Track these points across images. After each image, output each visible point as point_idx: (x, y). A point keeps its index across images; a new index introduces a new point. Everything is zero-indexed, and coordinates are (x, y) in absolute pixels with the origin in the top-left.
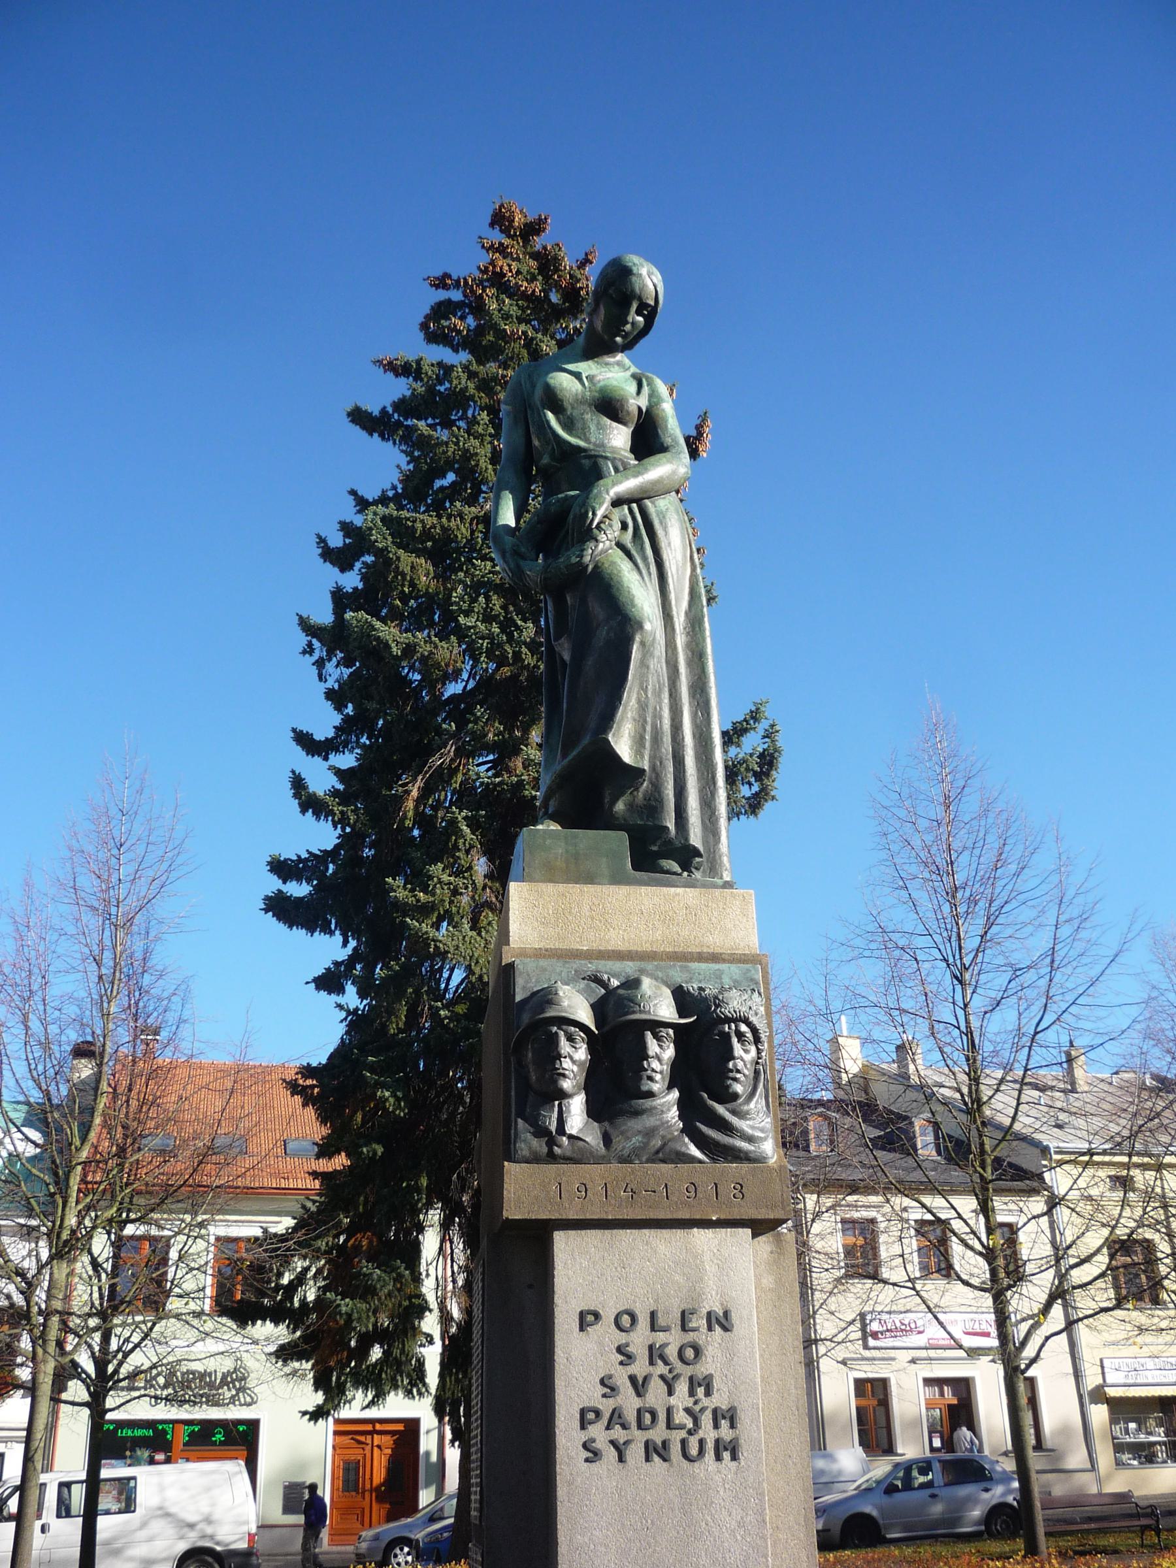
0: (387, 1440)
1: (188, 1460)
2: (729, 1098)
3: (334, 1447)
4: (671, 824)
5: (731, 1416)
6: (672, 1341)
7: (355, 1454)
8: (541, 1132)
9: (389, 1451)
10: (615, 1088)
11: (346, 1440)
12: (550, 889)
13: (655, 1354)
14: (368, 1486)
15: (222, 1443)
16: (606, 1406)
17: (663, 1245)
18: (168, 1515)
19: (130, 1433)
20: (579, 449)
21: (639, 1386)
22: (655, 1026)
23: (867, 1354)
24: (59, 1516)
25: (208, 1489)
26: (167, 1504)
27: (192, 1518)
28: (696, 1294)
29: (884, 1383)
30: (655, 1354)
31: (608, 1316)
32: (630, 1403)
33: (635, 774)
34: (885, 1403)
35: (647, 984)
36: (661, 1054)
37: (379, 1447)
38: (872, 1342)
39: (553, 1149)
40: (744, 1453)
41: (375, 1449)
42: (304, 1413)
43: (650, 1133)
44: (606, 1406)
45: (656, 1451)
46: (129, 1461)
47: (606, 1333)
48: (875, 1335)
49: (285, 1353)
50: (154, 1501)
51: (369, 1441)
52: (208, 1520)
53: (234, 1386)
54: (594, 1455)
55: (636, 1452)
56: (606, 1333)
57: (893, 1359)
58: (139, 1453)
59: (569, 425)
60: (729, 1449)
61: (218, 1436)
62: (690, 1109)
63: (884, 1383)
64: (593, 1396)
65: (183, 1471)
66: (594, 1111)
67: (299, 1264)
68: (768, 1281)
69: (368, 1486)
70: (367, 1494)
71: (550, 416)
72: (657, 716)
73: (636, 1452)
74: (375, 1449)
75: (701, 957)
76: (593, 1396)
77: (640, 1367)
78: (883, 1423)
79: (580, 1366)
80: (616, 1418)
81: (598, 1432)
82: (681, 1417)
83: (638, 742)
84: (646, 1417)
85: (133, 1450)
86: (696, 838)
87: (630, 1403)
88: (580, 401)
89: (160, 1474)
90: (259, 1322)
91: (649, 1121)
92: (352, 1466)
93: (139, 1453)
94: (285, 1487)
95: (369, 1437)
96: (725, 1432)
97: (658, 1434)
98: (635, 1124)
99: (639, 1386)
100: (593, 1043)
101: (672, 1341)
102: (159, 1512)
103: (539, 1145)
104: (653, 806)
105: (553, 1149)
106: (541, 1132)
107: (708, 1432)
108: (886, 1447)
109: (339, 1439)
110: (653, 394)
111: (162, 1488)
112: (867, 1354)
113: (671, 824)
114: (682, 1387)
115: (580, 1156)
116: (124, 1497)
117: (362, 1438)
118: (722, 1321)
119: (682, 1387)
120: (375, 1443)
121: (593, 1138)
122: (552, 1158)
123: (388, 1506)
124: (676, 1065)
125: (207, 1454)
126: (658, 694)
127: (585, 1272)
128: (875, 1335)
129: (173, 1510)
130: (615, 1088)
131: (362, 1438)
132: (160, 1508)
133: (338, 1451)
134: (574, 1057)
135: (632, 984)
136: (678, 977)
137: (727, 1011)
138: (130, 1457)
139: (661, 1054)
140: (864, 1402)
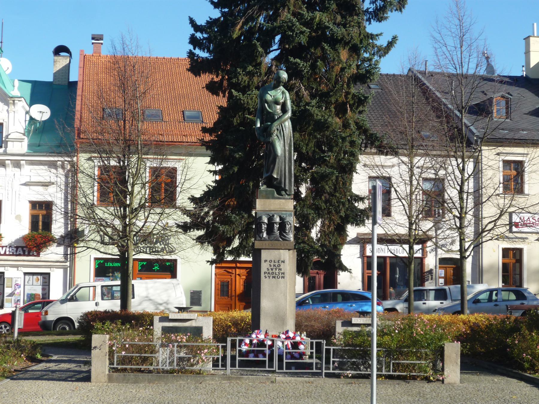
0: (244, 272)
1: (141, 279)
2: (286, 233)
3: (215, 274)
4: (283, 186)
5: (284, 273)
6: (277, 264)
7: (227, 278)
8: (260, 237)
9: (244, 277)
10: (270, 230)
11: (222, 271)
12: (262, 200)
13: (274, 266)
14: (233, 294)
15: (158, 271)
16: (268, 272)
17: (276, 252)
18: (150, 300)
19: (111, 265)
20: (271, 112)
21: (272, 269)
22: (276, 223)
23: (511, 235)
24: (102, 299)
25: (166, 290)
26: (149, 295)
27: (161, 302)
28: (280, 258)
29: (520, 251)
30: (274, 266)
31: (268, 261)
32: (271, 271)
33: (277, 179)
34: (520, 261)
35: (275, 216)
36: (276, 226)
37: (239, 275)
38: (514, 229)
39: (261, 239)
40: (285, 278)
41: (237, 276)
42: (208, 262)
43: (275, 237)
44: (268, 272)
45: (274, 277)
46: (111, 278)
47: (268, 263)
48: (517, 225)
49: (200, 240)
50: (144, 294)
51: (234, 272)
52: (167, 303)
53: (163, 243)
54: (266, 277)
55: (271, 277)
56: (268, 263)
57: (527, 238)
58: (116, 274)
59: (269, 107)
60: (283, 277)
61: (156, 267)
62: (281, 234)
63: (520, 251)
64: (266, 270)
65: (156, 282)
66: (267, 234)
67: (206, 209)
68: (291, 256)
69: (233, 294)
70: (233, 298)
71: (266, 105)
72: (281, 167)
73: (271, 277)
74: (237, 276)
75: (284, 211)
76: (266, 270)
77: (272, 267)
78: (518, 272)
79: (264, 267)
80: (269, 273)
81: (266, 275)
82: (277, 273)
83: (277, 174)
84: (273, 273)
85: (113, 273)
86: (287, 188)
87: (271, 271)
88: (271, 102)
89: (146, 283)
90: (192, 230)
91: (274, 236)
92: (225, 284)
93: (116, 274)
94: (191, 293)
95: (234, 270)
96: (283, 275)
97: (274, 275)
98: (272, 236)
99: (272, 269)
100: (267, 224)
101: (277, 264)
102: (146, 299)
103: (259, 239)
104: (280, 183)
105: (261, 239)
106: (260, 237)
107: (281, 275)
108: (518, 284)
109: (218, 270)
110: (286, 98)
111: (147, 289)
112: (511, 235)
113: (283, 186)
114: (278, 270)
115: (265, 240)
116: (110, 295)
117: (230, 271)
118: (283, 262)
119: (278, 270)
120: (237, 273)
121: (267, 238)
122: (261, 240)
123: (244, 304)
124: (279, 227)
125: (151, 276)
126: (282, 164)
127: (265, 255)
128: (517, 225)
129: (152, 298)
130: (270, 230)
131: (230, 271)
132: (147, 297)
133: (218, 277)
134: (264, 227)
135: (273, 216)
136: (280, 214)
137: (286, 221)
138: (112, 276)
139: (276, 226)
140: (507, 261)
